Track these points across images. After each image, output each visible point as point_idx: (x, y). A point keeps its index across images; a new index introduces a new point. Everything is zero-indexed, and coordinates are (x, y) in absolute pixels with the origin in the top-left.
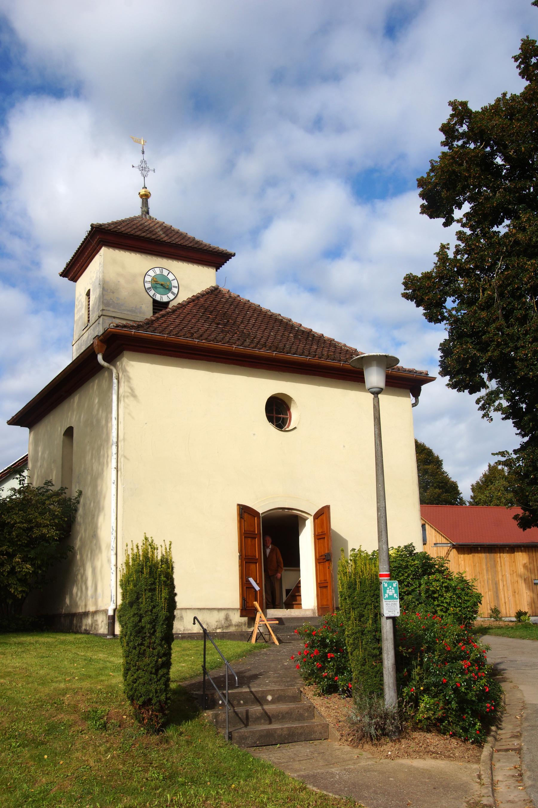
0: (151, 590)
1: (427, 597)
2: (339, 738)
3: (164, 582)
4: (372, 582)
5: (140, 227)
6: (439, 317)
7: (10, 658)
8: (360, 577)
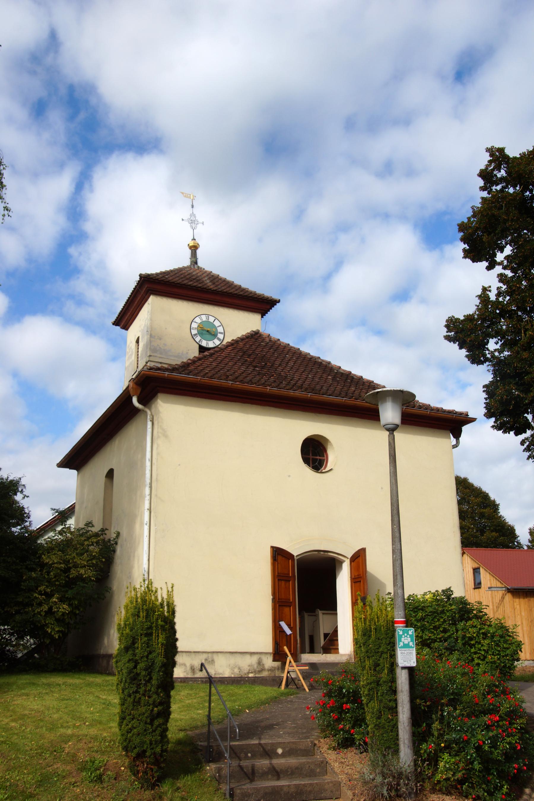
0: (147, 635)
1: (464, 644)
2: (351, 797)
3: (162, 626)
4: (388, 629)
5: (188, 277)
6: (482, 359)
7: (32, 699)
8: (375, 623)
